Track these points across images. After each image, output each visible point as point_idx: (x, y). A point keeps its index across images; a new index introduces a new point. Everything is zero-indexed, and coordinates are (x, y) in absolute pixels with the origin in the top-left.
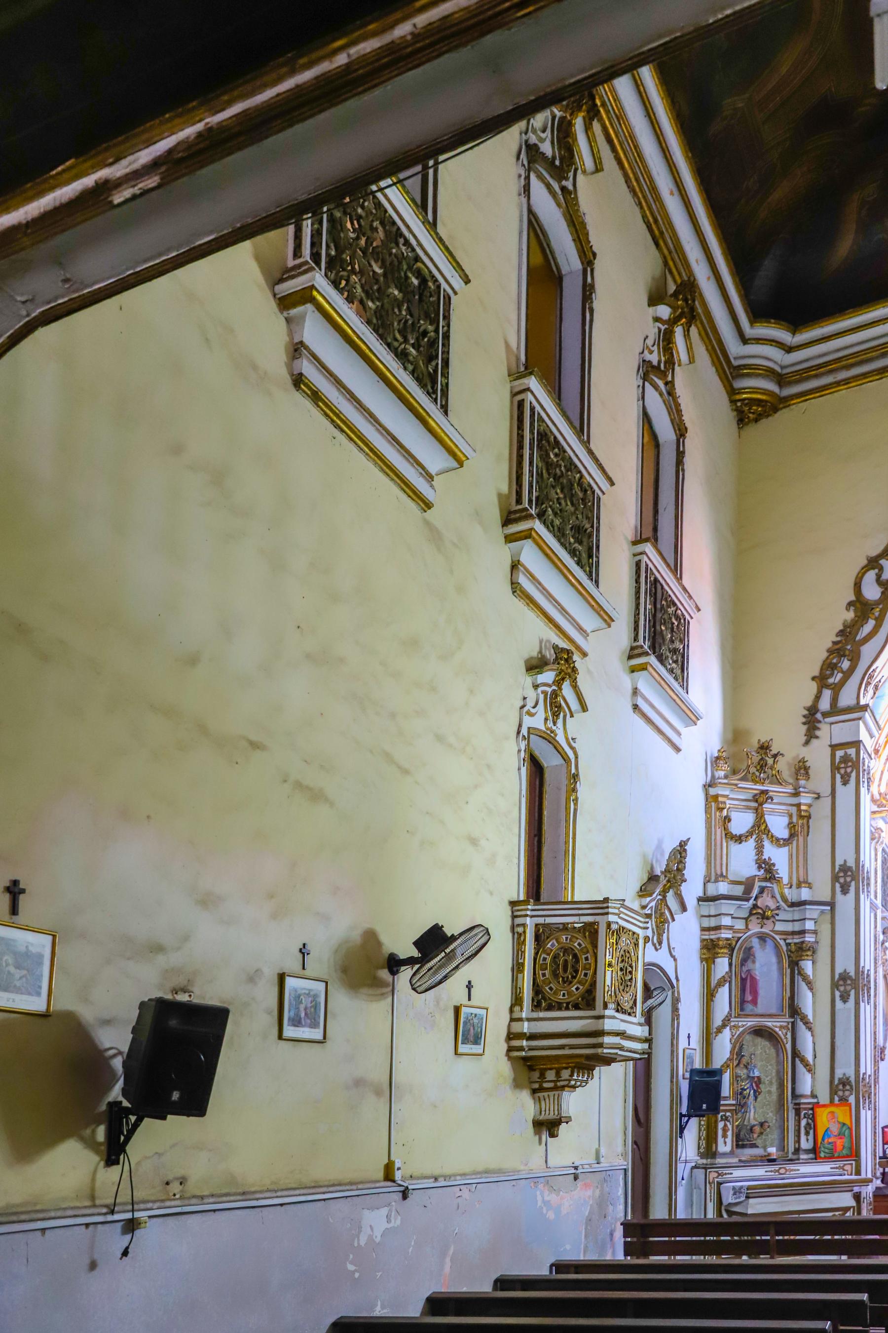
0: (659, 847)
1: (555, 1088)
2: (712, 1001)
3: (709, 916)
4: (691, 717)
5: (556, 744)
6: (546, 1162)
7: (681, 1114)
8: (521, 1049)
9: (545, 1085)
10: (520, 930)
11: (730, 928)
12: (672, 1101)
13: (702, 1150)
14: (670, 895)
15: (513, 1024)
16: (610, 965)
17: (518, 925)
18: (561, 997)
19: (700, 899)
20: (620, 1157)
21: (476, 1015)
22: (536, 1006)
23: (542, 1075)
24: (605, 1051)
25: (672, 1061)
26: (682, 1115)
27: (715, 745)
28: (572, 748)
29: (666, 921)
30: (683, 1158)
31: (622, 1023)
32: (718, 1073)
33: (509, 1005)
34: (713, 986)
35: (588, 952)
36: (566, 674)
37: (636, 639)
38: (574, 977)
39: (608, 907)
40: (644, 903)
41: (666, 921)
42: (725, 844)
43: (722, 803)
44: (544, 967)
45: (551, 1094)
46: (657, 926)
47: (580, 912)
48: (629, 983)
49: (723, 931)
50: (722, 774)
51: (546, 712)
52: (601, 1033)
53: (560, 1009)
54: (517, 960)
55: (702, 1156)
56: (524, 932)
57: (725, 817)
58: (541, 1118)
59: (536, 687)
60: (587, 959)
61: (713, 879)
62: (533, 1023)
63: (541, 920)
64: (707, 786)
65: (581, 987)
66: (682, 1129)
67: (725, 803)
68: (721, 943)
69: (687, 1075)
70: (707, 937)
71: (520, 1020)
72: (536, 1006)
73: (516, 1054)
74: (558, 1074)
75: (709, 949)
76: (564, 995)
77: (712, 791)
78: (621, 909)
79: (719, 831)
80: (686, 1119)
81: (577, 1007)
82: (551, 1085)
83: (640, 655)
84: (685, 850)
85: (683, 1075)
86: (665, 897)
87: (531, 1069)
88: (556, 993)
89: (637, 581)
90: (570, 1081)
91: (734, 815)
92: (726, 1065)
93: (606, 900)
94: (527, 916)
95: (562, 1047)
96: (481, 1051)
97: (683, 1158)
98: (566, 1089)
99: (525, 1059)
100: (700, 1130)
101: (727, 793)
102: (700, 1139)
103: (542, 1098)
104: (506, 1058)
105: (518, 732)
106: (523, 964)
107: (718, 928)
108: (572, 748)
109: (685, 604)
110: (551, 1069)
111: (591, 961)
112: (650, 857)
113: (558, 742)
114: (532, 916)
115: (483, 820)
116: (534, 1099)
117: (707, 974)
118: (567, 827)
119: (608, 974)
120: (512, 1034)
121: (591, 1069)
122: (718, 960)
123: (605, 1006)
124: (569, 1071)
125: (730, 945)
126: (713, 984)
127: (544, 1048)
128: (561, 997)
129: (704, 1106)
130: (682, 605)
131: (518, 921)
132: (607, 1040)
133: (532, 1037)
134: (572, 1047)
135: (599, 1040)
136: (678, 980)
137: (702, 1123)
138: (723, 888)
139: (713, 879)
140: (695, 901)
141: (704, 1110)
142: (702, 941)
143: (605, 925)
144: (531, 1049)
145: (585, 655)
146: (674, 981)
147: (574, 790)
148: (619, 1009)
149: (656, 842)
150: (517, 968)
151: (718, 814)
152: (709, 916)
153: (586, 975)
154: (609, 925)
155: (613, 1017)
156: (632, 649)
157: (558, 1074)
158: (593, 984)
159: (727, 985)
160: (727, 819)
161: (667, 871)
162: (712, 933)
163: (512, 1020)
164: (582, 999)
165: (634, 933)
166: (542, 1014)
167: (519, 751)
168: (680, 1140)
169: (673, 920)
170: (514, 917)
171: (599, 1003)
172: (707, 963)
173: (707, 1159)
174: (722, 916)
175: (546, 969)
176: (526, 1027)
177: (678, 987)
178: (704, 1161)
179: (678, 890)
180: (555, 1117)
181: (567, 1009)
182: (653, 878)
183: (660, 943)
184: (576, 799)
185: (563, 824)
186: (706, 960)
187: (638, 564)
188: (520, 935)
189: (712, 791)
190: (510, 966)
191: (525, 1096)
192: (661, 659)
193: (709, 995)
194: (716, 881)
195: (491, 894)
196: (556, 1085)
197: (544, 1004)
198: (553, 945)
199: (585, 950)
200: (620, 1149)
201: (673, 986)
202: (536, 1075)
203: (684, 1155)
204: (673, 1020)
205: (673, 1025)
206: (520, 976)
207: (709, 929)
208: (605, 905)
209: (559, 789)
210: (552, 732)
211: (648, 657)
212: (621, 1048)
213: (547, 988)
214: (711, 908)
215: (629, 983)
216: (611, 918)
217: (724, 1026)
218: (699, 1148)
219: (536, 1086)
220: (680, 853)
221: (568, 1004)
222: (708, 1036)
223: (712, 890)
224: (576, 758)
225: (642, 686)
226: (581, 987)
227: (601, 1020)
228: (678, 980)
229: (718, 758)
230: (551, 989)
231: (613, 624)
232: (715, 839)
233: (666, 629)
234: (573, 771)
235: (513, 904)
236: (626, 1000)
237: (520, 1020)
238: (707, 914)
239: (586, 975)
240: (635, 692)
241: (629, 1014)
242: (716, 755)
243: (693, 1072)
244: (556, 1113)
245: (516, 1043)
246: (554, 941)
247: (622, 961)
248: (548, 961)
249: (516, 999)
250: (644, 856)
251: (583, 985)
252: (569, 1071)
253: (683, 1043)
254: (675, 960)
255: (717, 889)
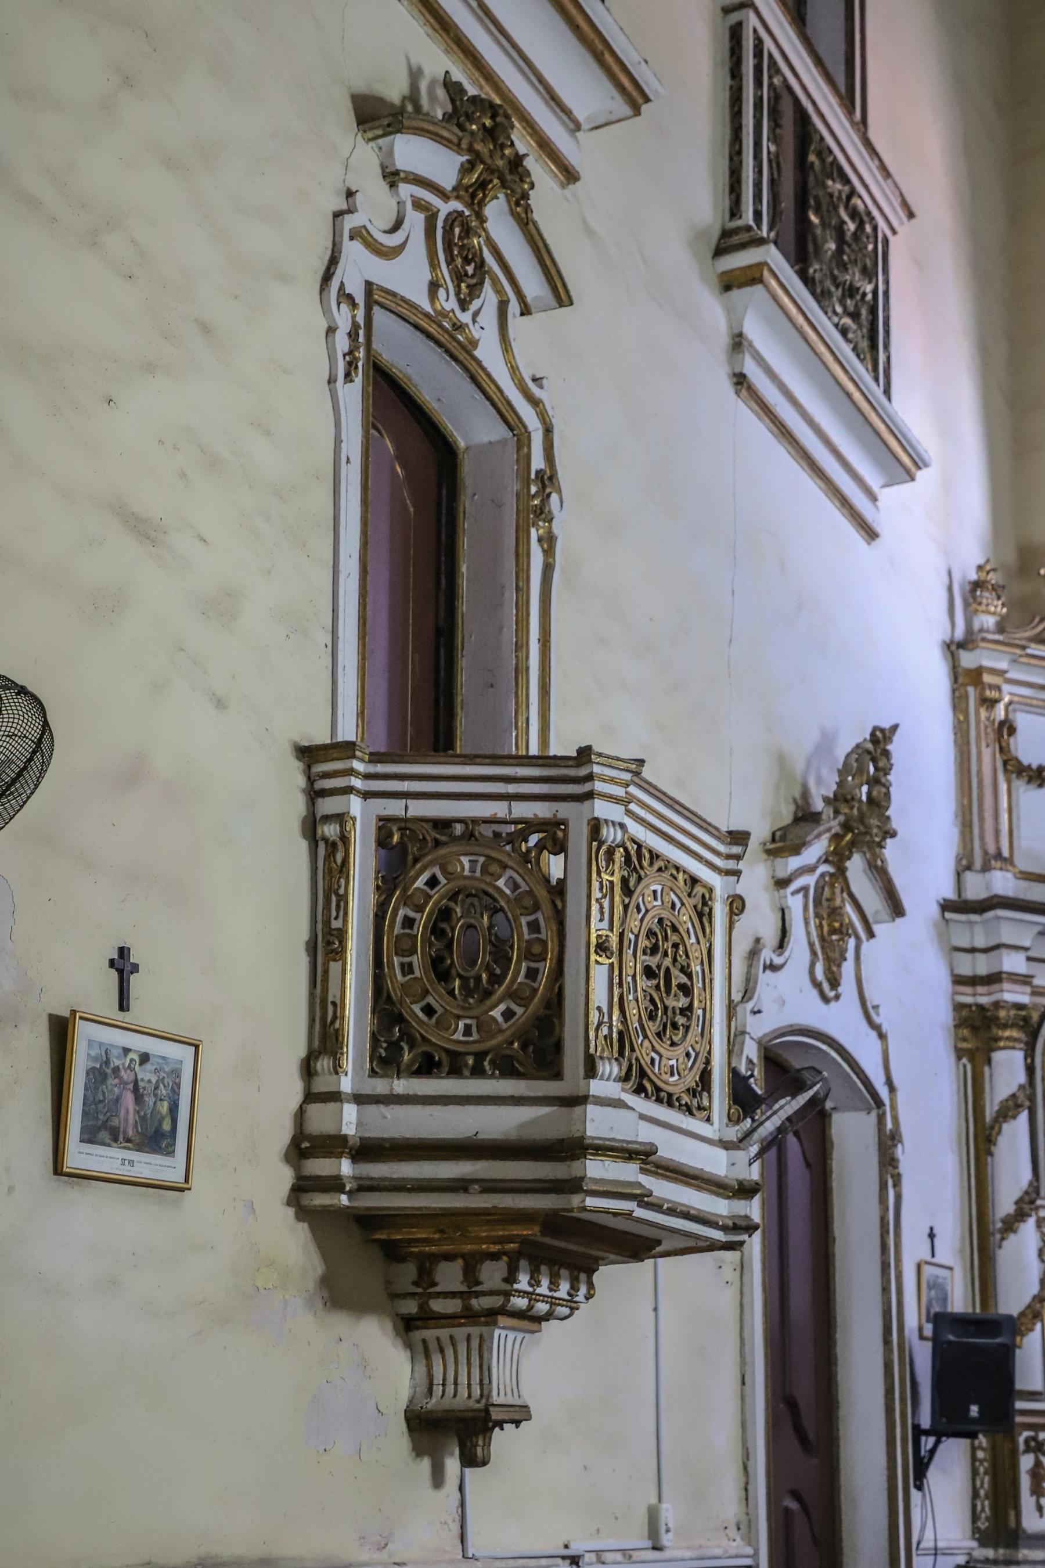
0: (826, 742)
1: (470, 1316)
2: (990, 1154)
3: (973, 950)
4: (902, 462)
5: (472, 366)
6: (463, 1538)
7: (916, 1428)
8: (334, 1184)
9: (437, 1306)
10: (330, 830)
11: (1025, 980)
12: (889, 1391)
13: (983, 1525)
14: (856, 865)
15: (313, 1109)
16: (602, 947)
17: (327, 819)
18: (459, 1036)
19: (946, 906)
20: (732, 1532)
21: (145, 1058)
22: (385, 1059)
23: (425, 1277)
24: (590, 1202)
25: (885, 1290)
26: (918, 1432)
27: (971, 552)
28: (535, 402)
29: (844, 931)
30: (928, 1543)
31: (643, 1124)
32: (1013, 1328)
33: (302, 1052)
34: (989, 1116)
35: (536, 907)
36: (490, 170)
37: (735, 211)
38: (496, 979)
39: (590, 777)
40: (781, 874)
41: (844, 931)
42: (1003, 787)
43: (991, 687)
44: (406, 944)
45: (460, 1333)
46: (822, 939)
47: (512, 789)
48: (681, 1020)
49: (1006, 986)
50: (989, 621)
51: (434, 264)
52: (576, 1148)
53: (455, 1071)
54: (327, 923)
55: (983, 1538)
56: (345, 839)
57: (1002, 724)
58: (432, 1403)
59: (392, 177)
60: (534, 927)
61: (978, 863)
62: (372, 1109)
63: (395, 808)
64: (953, 648)
65: (519, 1010)
66: (921, 1467)
67: (998, 688)
68: (1002, 1014)
69: (928, 1329)
70: (969, 1000)
71: (335, 1097)
72: (384, 1062)
73: (320, 1200)
74: (470, 1274)
75: (974, 1029)
76: (467, 1031)
77: (968, 660)
78: (632, 789)
79: (987, 754)
80: (932, 1440)
81: (508, 1069)
82: (452, 1306)
83: (743, 246)
84: (886, 754)
85: (920, 1329)
86: (841, 872)
87: (392, 1252)
88: (442, 1025)
89: (736, 73)
90: (507, 1294)
91: (1022, 720)
92: (1032, 1314)
93: (585, 754)
94: (349, 790)
95: (461, 1186)
96: (176, 1176)
97: (928, 1543)
98: (502, 1320)
99: (367, 1222)
100: (975, 1472)
101: (1003, 665)
102: (975, 1495)
103: (433, 1346)
104: (290, 1212)
105: (327, 277)
106: (341, 935)
107: (994, 979)
108: (535, 402)
109: (876, 195)
110: (449, 1257)
111: (547, 933)
112: (800, 766)
113: (479, 363)
114: (367, 795)
115: (183, 475)
116: (409, 1345)
117: (975, 1089)
118: (522, 607)
119: (599, 976)
120: (311, 1138)
121: (583, 1269)
122: (998, 1056)
123: (591, 1071)
124: (503, 1263)
125: (1026, 1019)
126: (989, 1116)
127: (414, 1188)
128: (459, 1036)
129: (974, 1410)
130: (866, 187)
131: (328, 806)
132: (596, 1169)
133: (367, 1150)
134: (490, 1187)
135: (573, 1169)
136: (892, 1089)
137: (980, 1454)
138: (1002, 883)
139: (978, 863)
140: (935, 910)
141: (974, 1421)
142: (958, 1007)
143: (585, 830)
144: (366, 1186)
145: (569, 175)
146: (884, 1092)
147: (542, 513)
148: (640, 1080)
149: (815, 735)
150: (325, 945)
151: (983, 713)
152: (973, 950)
153: (532, 974)
154: (596, 826)
155: (619, 1104)
156: (725, 234)
157: (470, 1274)
158: (555, 1002)
159: (1024, 1116)
160: (1007, 728)
161: (840, 799)
162: (980, 989)
163: (310, 1097)
164: (524, 1047)
165: (694, 881)
166: (401, 1086)
167: (331, 330)
168: (915, 1495)
169: (871, 934)
170: (314, 794)
171: (572, 1059)
172: (972, 1060)
173: (996, 1546)
174: (1004, 952)
175: (413, 951)
176: (349, 1120)
177: (894, 1108)
178: (990, 1553)
179: (875, 856)
180: (472, 1404)
181: (478, 1072)
182: (806, 816)
183: (834, 983)
184: (549, 542)
185: (510, 595)
186: (971, 1055)
187: (736, 33)
188: (332, 847)
189: (968, 660)
190: (304, 935)
191: (375, 1340)
192: (801, 257)
193: (981, 1139)
194: (986, 868)
195: (220, 704)
196: (467, 1308)
197: (406, 1057)
198: (433, 882)
199: (528, 902)
200: (731, 1509)
201: (879, 1103)
202: (408, 1272)
203: (929, 1534)
204: (883, 1187)
205: (883, 1200)
206: (334, 967)
207: (973, 981)
208: (583, 772)
209: (498, 505)
210: (459, 327)
211: (762, 249)
212: (643, 1199)
213: (417, 1009)
214: (974, 931)
215: (681, 1020)
216: (602, 809)
217: (1020, 1215)
218: (975, 1518)
219: (411, 1307)
220: (874, 760)
221: (480, 1056)
222: (985, 1238)
223: (976, 888)
224: (548, 431)
225: (754, 330)
226: (519, 1010)
227: (578, 1110)
228: (892, 1089)
229: (977, 585)
230: (429, 1011)
231: (645, 108)
232: (980, 772)
233: (824, 224)
234: (538, 462)
235: (308, 754)
236: (671, 1064)
237: (335, 1097)
238: (966, 944)
239: (532, 974)
240: (738, 343)
241: (689, 1110)
242: (973, 576)
243: (942, 1321)
244: (476, 1391)
245: (319, 1167)
246: (437, 870)
247: (654, 950)
248: (419, 929)
249: (324, 1037)
250: (781, 761)
251: (524, 1002)
252: (503, 1263)
253: (913, 1249)
254: (882, 1036)
255: (988, 885)
